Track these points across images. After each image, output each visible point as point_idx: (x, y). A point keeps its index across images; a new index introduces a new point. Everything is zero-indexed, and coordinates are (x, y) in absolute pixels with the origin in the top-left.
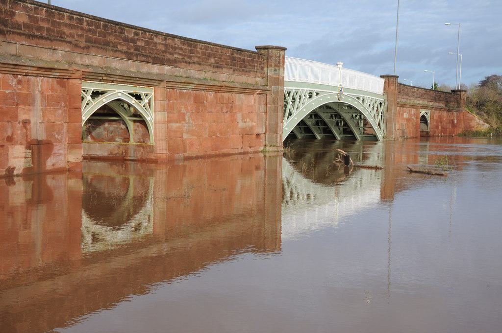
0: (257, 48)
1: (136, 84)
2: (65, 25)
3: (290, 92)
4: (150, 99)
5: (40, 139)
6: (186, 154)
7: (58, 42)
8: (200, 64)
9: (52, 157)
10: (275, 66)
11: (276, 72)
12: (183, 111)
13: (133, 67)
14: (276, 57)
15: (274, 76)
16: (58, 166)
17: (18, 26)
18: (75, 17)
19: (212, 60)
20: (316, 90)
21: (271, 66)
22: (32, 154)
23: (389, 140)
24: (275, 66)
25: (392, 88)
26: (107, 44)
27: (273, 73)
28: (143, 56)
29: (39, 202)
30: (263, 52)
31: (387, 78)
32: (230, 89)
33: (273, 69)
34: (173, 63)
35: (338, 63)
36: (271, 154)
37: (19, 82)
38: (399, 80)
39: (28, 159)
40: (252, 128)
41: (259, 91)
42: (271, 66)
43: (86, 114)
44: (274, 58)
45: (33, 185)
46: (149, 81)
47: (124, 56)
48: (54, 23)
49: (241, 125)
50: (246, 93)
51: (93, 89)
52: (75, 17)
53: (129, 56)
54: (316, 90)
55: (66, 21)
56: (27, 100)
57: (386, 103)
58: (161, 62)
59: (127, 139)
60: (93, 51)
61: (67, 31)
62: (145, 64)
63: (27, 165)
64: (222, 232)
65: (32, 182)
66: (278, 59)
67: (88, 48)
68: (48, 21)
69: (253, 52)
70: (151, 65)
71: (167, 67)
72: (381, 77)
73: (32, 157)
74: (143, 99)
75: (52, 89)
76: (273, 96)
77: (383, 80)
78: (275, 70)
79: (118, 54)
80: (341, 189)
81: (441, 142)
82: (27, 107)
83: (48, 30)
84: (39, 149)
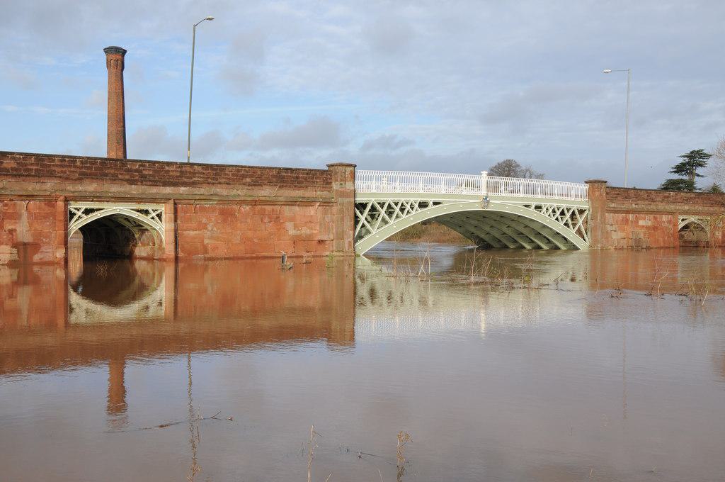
0: (328, 166)
1: (139, 203)
2: (57, 166)
5: (26, 241)
6: (207, 256)
8: (227, 184)
9: (39, 254)
10: (341, 180)
12: (203, 221)
13: (135, 190)
16: (45, 260)
17: (7, 170)
18: (67, 159)
19: (248, 180)
22: (18, 251)
24: (341, 180)
25: (597, 194)
26: (106, 175)
27: (339, 186)
28: (150, 181)
29: (25, 283)
32: (273, 203)
34: (193, 184)
36: (338, 258)
37: (6, 205)
39: (431, 300)
40: (311, 235)
43: (680, 227)
45: (19, 272)
46: (154, 200)
47: (125, 183)
48: (43, 166)
49: (292, 232)
50: (289, 205)
51: (85, 207)
52: (67, 159)
53: (132, 182)
55: (57, 162)
56: (15, 217)
57: (591, 210)
58: (175, 185)
59: (154, 244)
60: (86, 181)
61: (58, 169)
62: (152, 187)
63: (13, 259)
64: (265, 323)
65: (17, 270)
67: (81, 179)
68: (37, 165)
69: (325, 171)
70: (161, 187)
71: (183, 188)
72: (586, 182)
73: (18, 254)
75: (40, 209)
77: (586, 187)
79: (117, 182)
80: (491, 299)
82: (13, 221)
83: (36, 170)
84: (25, 252)
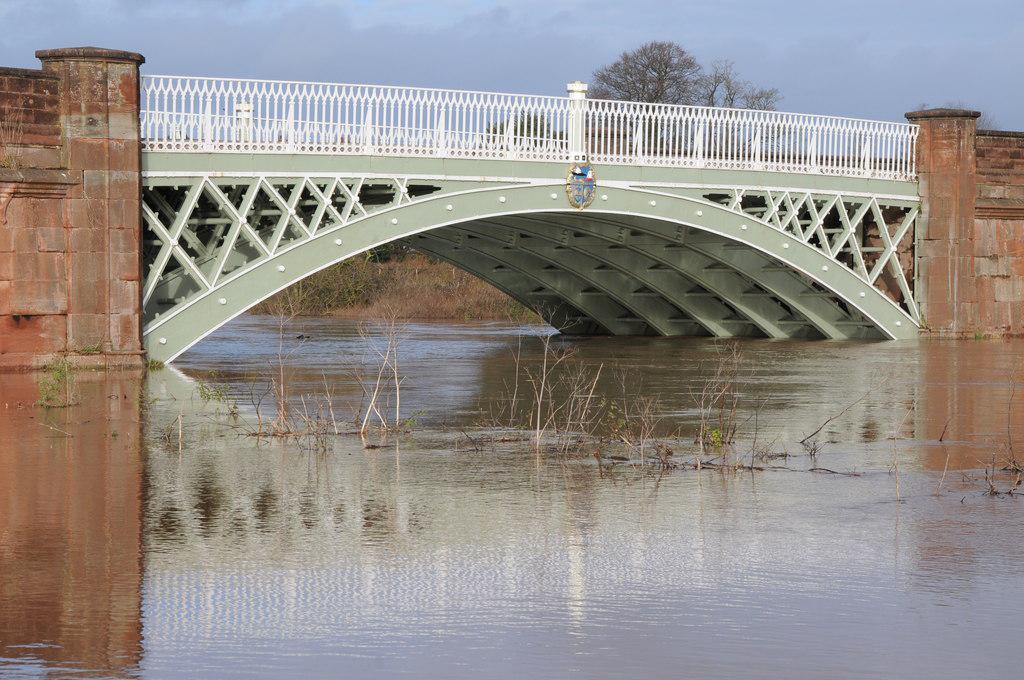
3: (325, 186)
4: (914, 221)
7: (932, 114)
10: (92, 109)
11: (95, 129)
14: (92, 81)
15: (89, 140)
20: (407, 177)
21: (78, 109)
23: (938, 339)
24: (92, 109)
27: (84, 129)
30: (55, 67)
31: (925, 122)
33: (84, 118)
35: (570, 87)
36: (84, 376)
38: (982, 124)
41: (13, 185)
42: (78, 109)
44: (84, 86)
54: (407, 177)
57: (926, 208)
66: (98, 88)
74: (844, 223)
76: (87, 199)
78: (92, 122)
81: (277, 369)
